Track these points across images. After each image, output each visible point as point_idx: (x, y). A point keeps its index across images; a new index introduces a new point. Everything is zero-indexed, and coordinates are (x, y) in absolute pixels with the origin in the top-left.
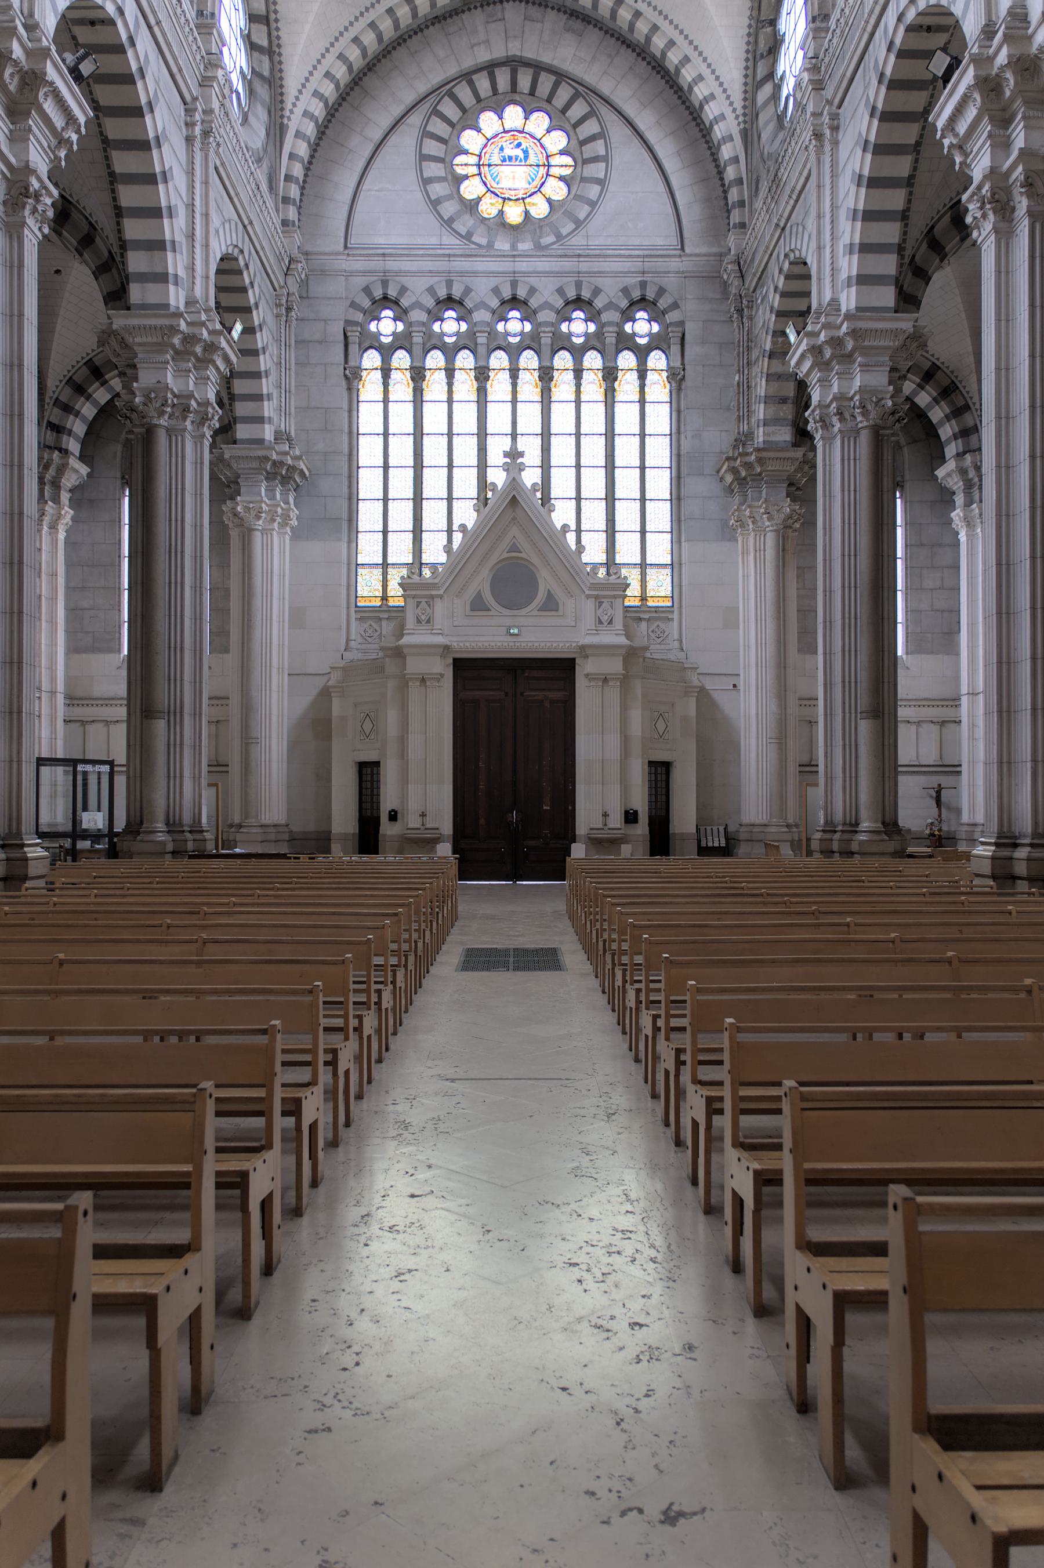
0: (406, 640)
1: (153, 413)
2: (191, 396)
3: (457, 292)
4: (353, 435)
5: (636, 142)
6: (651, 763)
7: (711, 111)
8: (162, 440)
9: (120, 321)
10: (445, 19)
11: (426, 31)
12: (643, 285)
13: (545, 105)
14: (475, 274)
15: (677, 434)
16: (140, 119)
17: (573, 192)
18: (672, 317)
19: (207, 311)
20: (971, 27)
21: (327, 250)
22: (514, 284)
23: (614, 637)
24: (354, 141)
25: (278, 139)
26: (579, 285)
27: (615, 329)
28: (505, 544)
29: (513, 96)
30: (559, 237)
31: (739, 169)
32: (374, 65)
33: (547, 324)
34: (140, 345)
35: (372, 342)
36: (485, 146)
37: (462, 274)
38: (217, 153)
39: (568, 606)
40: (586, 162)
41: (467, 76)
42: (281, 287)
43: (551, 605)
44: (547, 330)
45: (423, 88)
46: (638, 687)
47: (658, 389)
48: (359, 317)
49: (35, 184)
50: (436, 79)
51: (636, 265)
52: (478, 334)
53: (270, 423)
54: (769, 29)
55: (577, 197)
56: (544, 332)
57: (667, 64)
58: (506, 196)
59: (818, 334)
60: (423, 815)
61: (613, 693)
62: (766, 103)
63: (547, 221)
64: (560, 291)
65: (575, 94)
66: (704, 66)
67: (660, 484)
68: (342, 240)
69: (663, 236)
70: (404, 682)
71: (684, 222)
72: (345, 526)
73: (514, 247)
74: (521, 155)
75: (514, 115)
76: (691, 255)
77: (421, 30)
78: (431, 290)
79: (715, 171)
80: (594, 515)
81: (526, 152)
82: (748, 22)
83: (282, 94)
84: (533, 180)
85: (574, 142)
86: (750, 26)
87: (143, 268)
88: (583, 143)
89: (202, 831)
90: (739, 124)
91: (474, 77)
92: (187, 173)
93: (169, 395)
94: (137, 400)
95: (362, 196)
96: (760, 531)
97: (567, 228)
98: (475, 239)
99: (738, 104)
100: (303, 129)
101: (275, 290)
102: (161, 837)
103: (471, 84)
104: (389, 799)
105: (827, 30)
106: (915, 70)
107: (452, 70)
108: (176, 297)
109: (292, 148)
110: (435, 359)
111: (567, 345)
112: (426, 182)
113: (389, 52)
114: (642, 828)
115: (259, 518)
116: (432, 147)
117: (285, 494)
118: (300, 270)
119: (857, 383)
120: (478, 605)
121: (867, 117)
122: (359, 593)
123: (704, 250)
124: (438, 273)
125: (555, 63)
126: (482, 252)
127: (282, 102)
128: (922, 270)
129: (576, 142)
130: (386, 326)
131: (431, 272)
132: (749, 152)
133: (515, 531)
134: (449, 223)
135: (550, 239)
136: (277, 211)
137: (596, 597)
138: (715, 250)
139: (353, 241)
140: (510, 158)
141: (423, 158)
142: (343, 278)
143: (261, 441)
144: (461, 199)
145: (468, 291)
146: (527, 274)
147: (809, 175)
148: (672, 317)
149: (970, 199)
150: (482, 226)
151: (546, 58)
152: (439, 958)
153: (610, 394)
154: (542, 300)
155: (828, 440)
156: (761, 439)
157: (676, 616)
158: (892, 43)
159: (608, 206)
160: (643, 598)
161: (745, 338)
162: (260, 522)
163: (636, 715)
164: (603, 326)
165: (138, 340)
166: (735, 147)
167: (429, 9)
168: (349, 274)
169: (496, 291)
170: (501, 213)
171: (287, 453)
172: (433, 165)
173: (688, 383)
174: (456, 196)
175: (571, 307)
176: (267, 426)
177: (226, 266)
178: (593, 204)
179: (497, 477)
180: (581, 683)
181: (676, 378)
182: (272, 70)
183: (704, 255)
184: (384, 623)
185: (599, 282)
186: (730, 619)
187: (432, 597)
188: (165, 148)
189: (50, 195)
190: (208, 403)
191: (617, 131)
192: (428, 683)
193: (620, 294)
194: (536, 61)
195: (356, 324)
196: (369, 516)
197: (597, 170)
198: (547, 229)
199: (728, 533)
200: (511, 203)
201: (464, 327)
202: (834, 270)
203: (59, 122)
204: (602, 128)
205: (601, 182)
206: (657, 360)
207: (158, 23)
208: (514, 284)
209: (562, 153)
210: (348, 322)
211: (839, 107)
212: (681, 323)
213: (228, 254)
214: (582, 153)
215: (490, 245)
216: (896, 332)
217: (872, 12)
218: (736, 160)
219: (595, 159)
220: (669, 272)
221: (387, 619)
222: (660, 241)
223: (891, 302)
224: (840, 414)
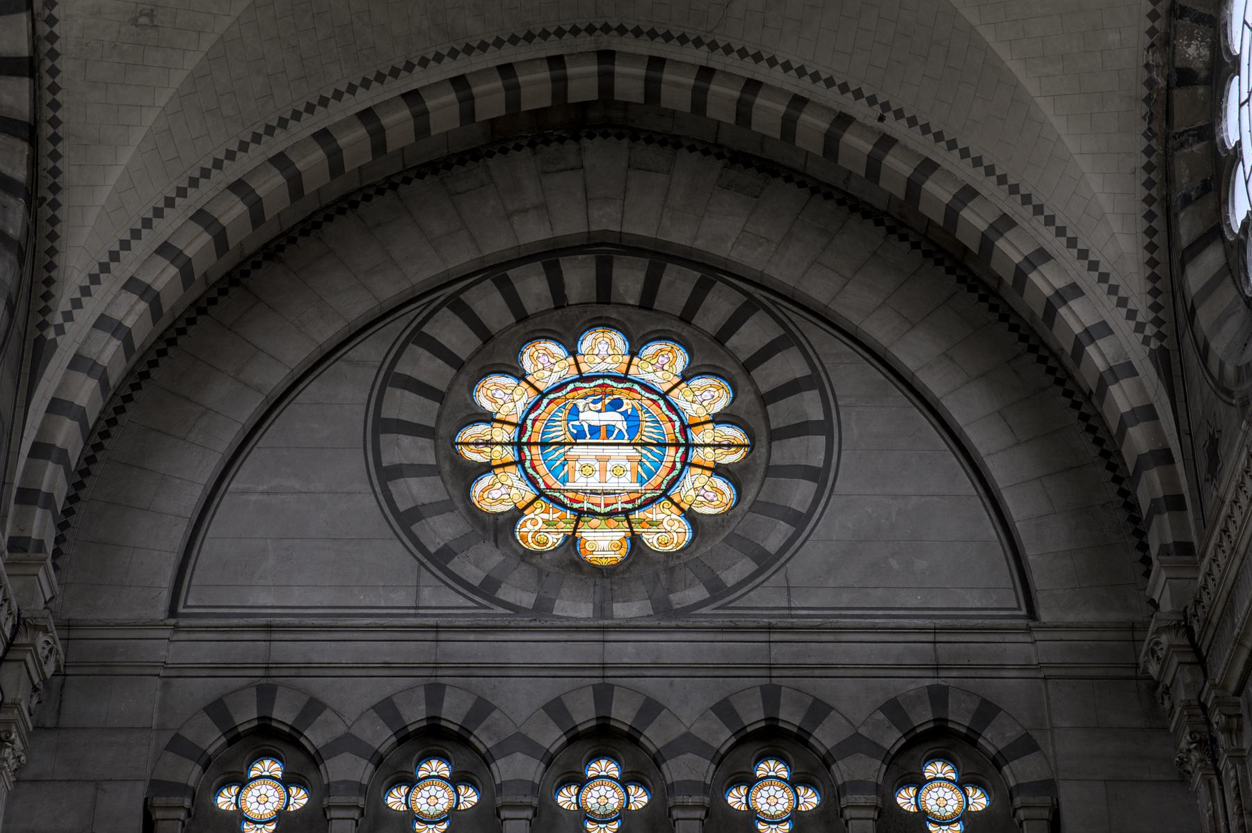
3: (453, 711)
5: (897, 397)
10: (448, 167)
11: (403, 189)
12: (938, 696)
13: (677, 327)
14: (502, 669)
17: (750, 498)
18: (1019, 771)
21: (123, 616)
22: (603, 694)
25: (26, 369)
26: (771, 696)
27: (872, 799)
30: (717, 590)
31: (1158, 433)
32: (281, 248)
33: (690, 787)
36: (536, 406)
37: (469, 669)
40: (776, 435)
44: (690, 801)
45: (389, 289)
48: (191, 773)
50: (423, 272)
51: (920, 650)
52: (505, 814)
54: (1197, 148)
55: (756, 507)
56: (684, 807)
57: (961, 235)
58: (586, 506)
62: (1210, 287)
65: (745, 304)
68: (165, 595)
71: (1031, 555)
73: (602, 610)
74: (622, 425)
76: (1056, 627)
77: (394, 187)
78: (386, 709)
79: (1094, 451)
81: (633, 420)
82: (1144, 143)
83: (49, 282)
84: (650, 474)
85: (748, 398)
86: (1149, 151)
88: (767, 399)
90: (1146, 341)
91: (511, 273)
97: (736, 570)
98: (507, 593)
99: (1141, 302)
100: (91, 352)
103: (505, 286)
107: (461, 257)
109: (60, 388)
112: (387, 474)
113: (317, 226)
118: (42, 652)
123: (1088, 615)
124: (406, 668)
125: (699, 244)
126: (524, 621)
127: (47, 296)
129: (752, 397)
131: (387, 666)
132: (1180, 396)
135: (698, 593)
138: (1113, 616)
139: (192, 600)
140: (595, 430)
141: (382, 426)
142: (159, 681)
144: (474, 513)
145: (482, 709)
146: (638, 670)
148: (1019, 771)
150: (524, 567)
151: (679, 235)
154: (676, 731)
161: (1232, 808)
164: (840, 791)
166: (1141, 388)
167: (411, 138)
168: (172, 673)
169: (556, 710)
170: (572, 541)
172: (406, 440)
174: (460, 506)
175: (753, 749)
178: (799, 521)
183: (1090, 627)
185: (824, 688)
193: (880, 716)
194: (655, 241)
200: (595, 522)
201: (469, 798)
204: (813, 367)
205: (818, 476)
208: (603, 694)
209: (718, 419)
210: (158, 787)
212: (1048, 786)
214: (767, 419)
215: (543, 607)
218: (1148, 413)
219: (802, 429)
220: (1002, 667)
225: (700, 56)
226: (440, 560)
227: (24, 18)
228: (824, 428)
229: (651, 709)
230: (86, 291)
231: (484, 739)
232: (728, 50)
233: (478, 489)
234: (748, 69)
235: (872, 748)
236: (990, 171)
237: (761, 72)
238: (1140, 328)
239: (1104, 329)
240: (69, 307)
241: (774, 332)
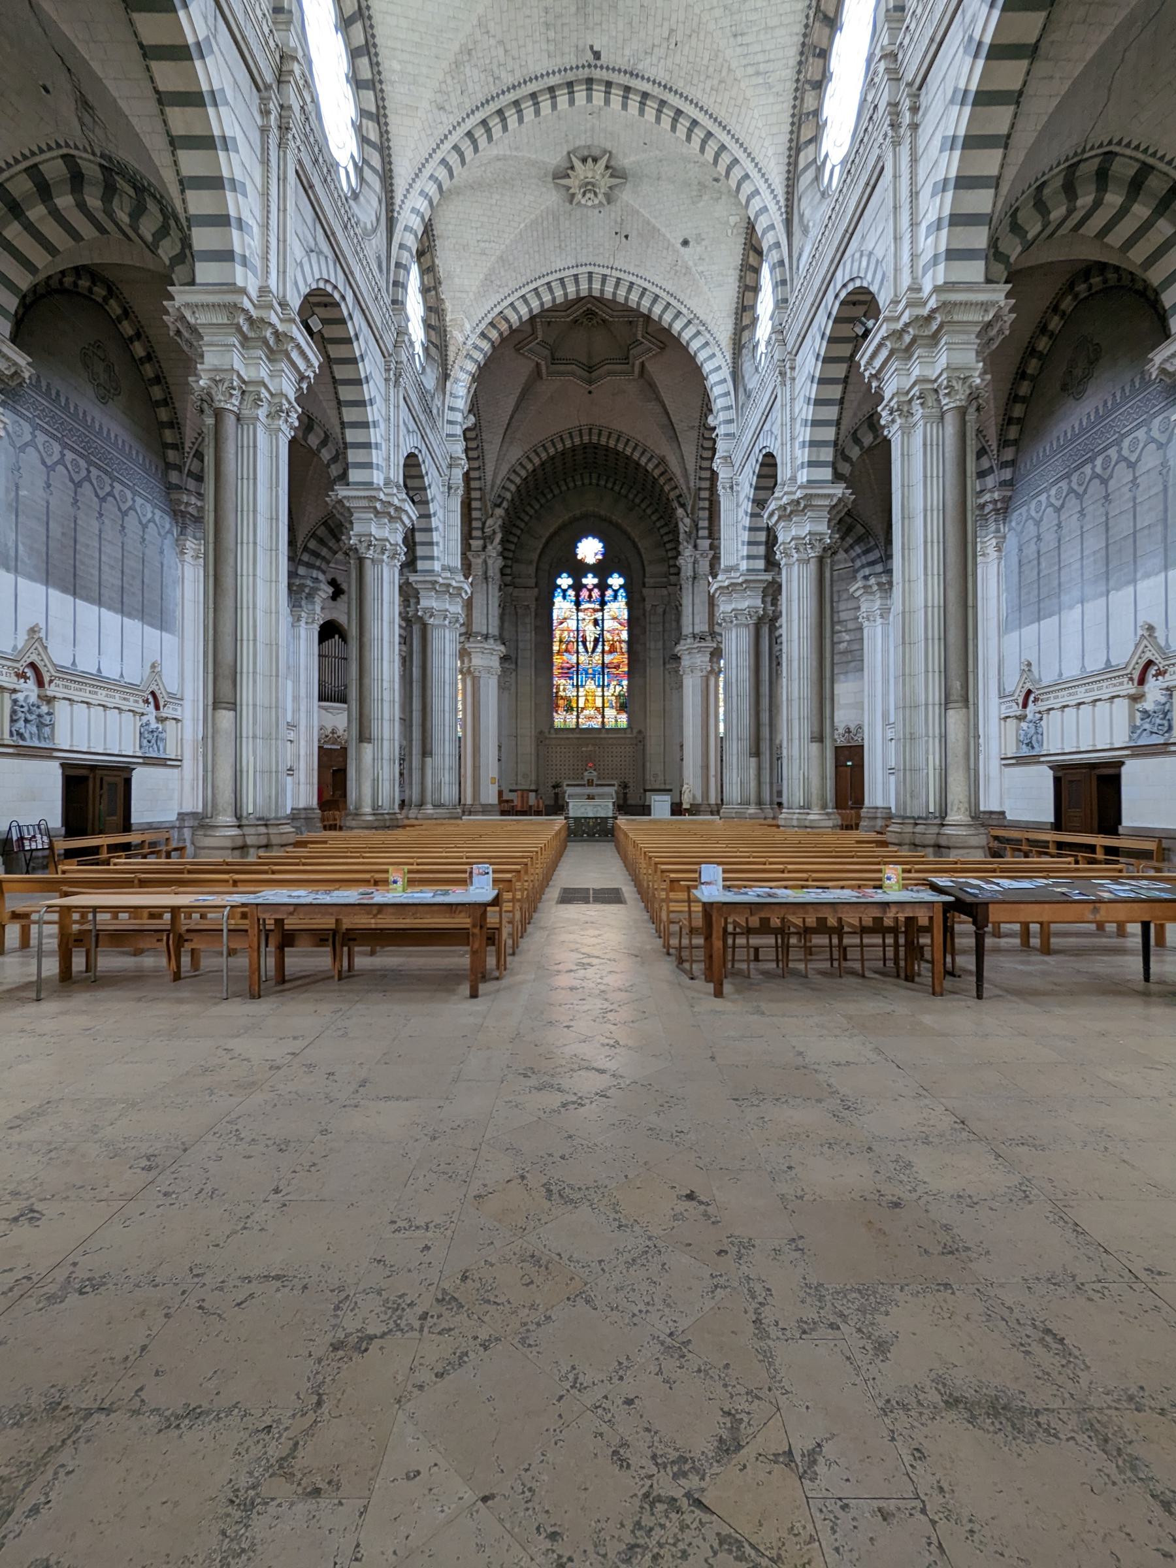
9: (412, 578)
16: (188, 63)
20: (883, 300)
42: (390, 355)
49: (286, 406)
66: (708, 336)
92: (262, 163)
93: (235, 377)
94: (201, 383)
101: (258, 90)
106: (846, 330)
108: (378, 478)
121: (814, 360)
128: (1021, 228)
143: (433, 571)
147: (883, 168)
149: (883, 409)
152: (544, 897)
158: (830, 314)
177: (410, 462)
189: (296, 411)
190: (397, 544)
202: (793, 459)
203: (302, 366)
216: (984, 306)
223: (829, 477)
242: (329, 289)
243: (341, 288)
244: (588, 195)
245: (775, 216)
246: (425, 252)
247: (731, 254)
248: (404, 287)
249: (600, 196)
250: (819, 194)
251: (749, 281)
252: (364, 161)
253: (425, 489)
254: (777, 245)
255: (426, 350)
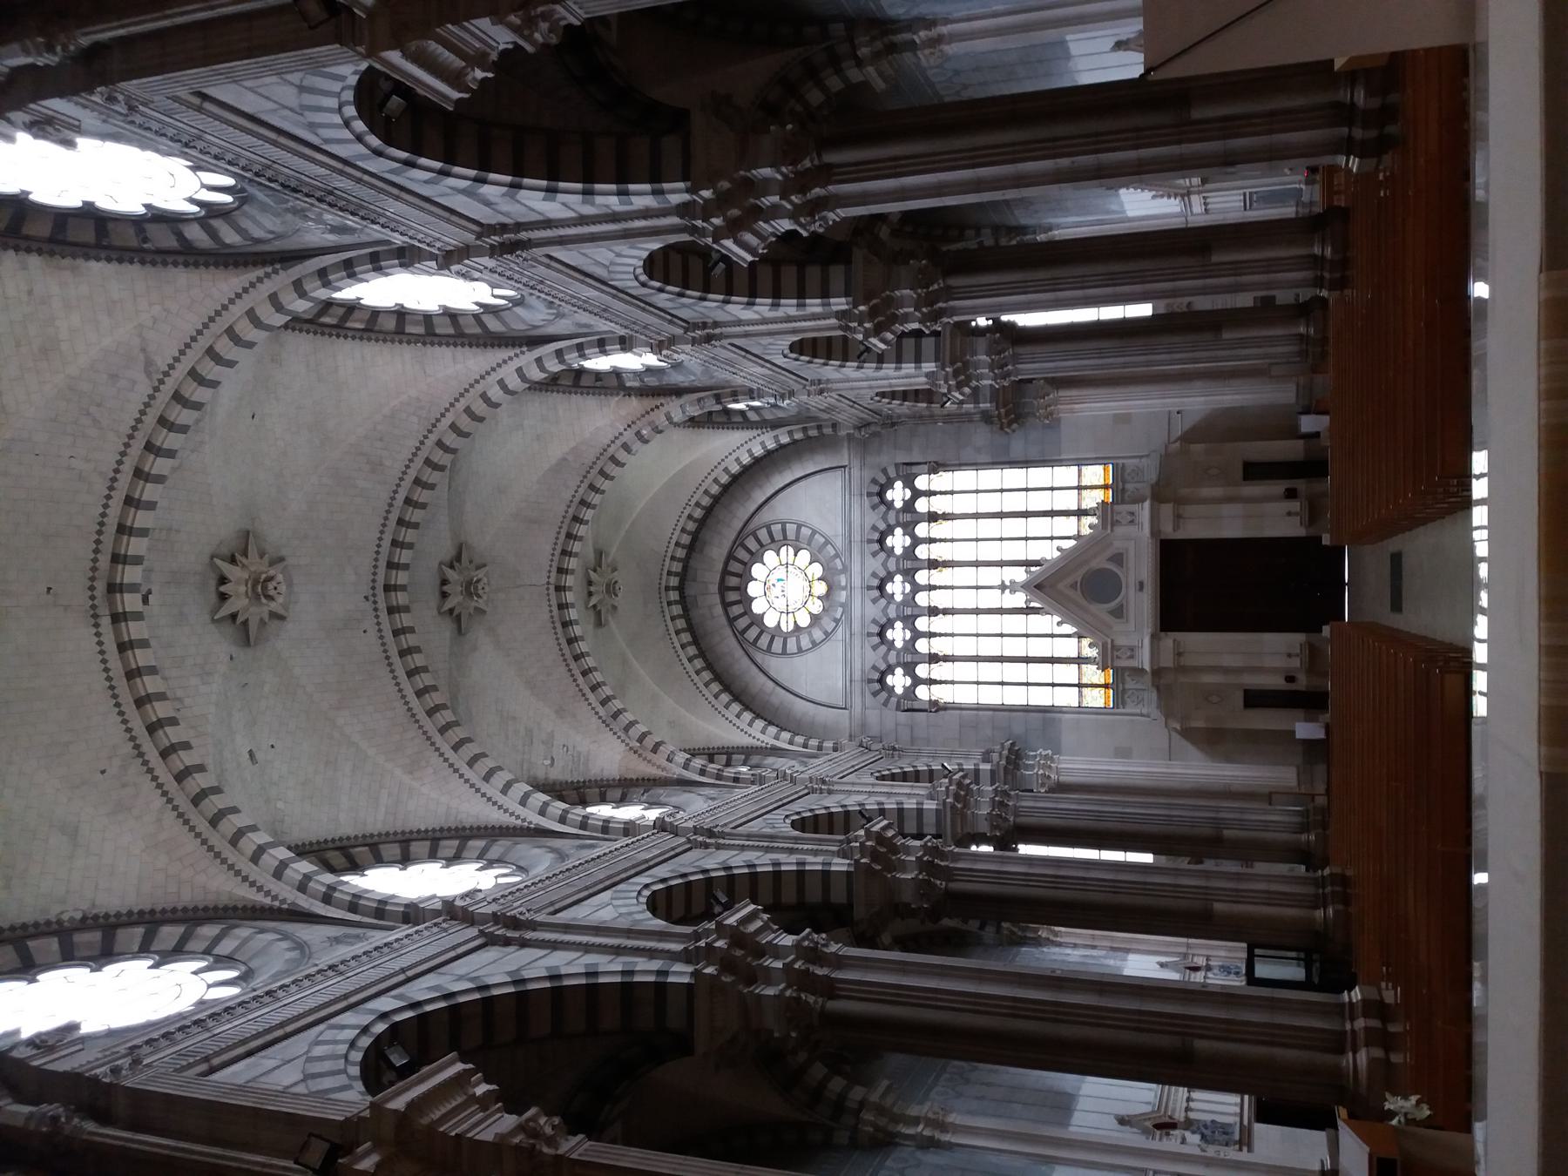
0: (1147, 667)
1: (1006, 825)
2: (993, 799)
4: (979, 708)
6: (1245, 478)
7: (758, 451)
8: (1022, 820)
12: (869, 495)
13: (748, 566)
14: (863, 616)
15: (977, 465)
18: (892, 473)
19: (849, 841)
23: (1145, 510)
24: (775, 700)
28: (1071, 593)
29: (742, 589)
30: (837, 556)
34: (962, 829)
35: (910, 692)
37: (863, 626)
38: (538, 911)
39: (1118, 545)
40: (785, 538)
41: (731, 621)
43: (1118, 559)
45: (739, 653)
46: (1184, 492)
47: (942, 480)
50: (733, 642)
53: (922, 804)
55: (809, 544)
59: (950, 385)
60: (1289, 655)
61: (1189, 510)
63: (825, 565)
64: (874, 554)
67: (1014, 477)
69: (836, 480)
70: (1181, 669)
71: (826, 467)
72: (1048, 715)
73: (844, 588)
75: (753, 589)
80: (1039, 526)
87: (914, 823)
89: (1308, 823)
95: (811, 696)
96: (1056, 402)
102: (1312, 837)
104: (1276, 682)
105: (759, 389)
107: (728, 632)
110: (922, 646)
111: (912, 549)
112: (800, 650)
114: (1300, 485)
115: (1049, 777)
116: (777, 646)
117: (1028, 758)
119: (984, 357)
120: (1118, 613)
122: (1103, 706)
130: (898, 681)
133: (1061, 586)
134: (827, 634)
136: (827, 754)
137: (1112, 525)
138: (846, 444)
139: (841, 704)
141: (784, 652)
144: (811, 626)
146: (863, 579)
147: (840, 395)
148: (892, 473)
151: (720, 566)
153: (947, 517)
155: (1018, 372)
156: (989, 405)
157: (1120, 461)
159: (816, 523)
160: (1105, 487)
162: (1052, 776)
163: (1206, 492)
165: (959, 831)
171: (1000, 754)
173: (940, 459)
176: (981, 767)
177: (662, 904)
179: (1019, 600)
180: (1180, 535)
181: (935, 468)
182: (742, 754)
184: (1127, 686)
185: (868, 527)
186: (1123, 419)
187: (1113, 646)
188: (527, 974)
191: (766, 516)
192: (1181, 650)
195: (898, 702)
196: (1041, 697)
197: (791, 529)
198: (831, 565)
199: (1054, 423)
206: (922, 482)
207: (403, 970)
208: (870, 588)
210: (898, 708)
211: (807, 380)
213: (647, 903)
215: (842, 605)
217: (769, 369)
218: (790, 433)
219: (784, 530)
221: (1123, 684)
222: (839, 483)
224: (1002, 367)
225: (668, 560)
226: (827, 634)
227: (381, 846)
228: (799, 527)
229: (874, 575)
230: (506, 811)
231: (883, 621)
232: (666, 551)
233: (802, 625)
234: (672, 546)
235: (886, 513)
236: (709, 474)
237: (673, 542)
238: (763, 433)
239: (519, 371)
240: (270, 898)
241: (751, 538)
242: (366, 1042)
243: (365, 1020)
244: (272, 593)
245: (527, 358)
246: (579, 792)
247: (564, 406)
248: (607, 821)
249: (272, 572)
250: (518, 310)
251: (390, 324)
252: (207, 952)
253: (847, 813)
254: (559, 354)
255: (490, 864)
